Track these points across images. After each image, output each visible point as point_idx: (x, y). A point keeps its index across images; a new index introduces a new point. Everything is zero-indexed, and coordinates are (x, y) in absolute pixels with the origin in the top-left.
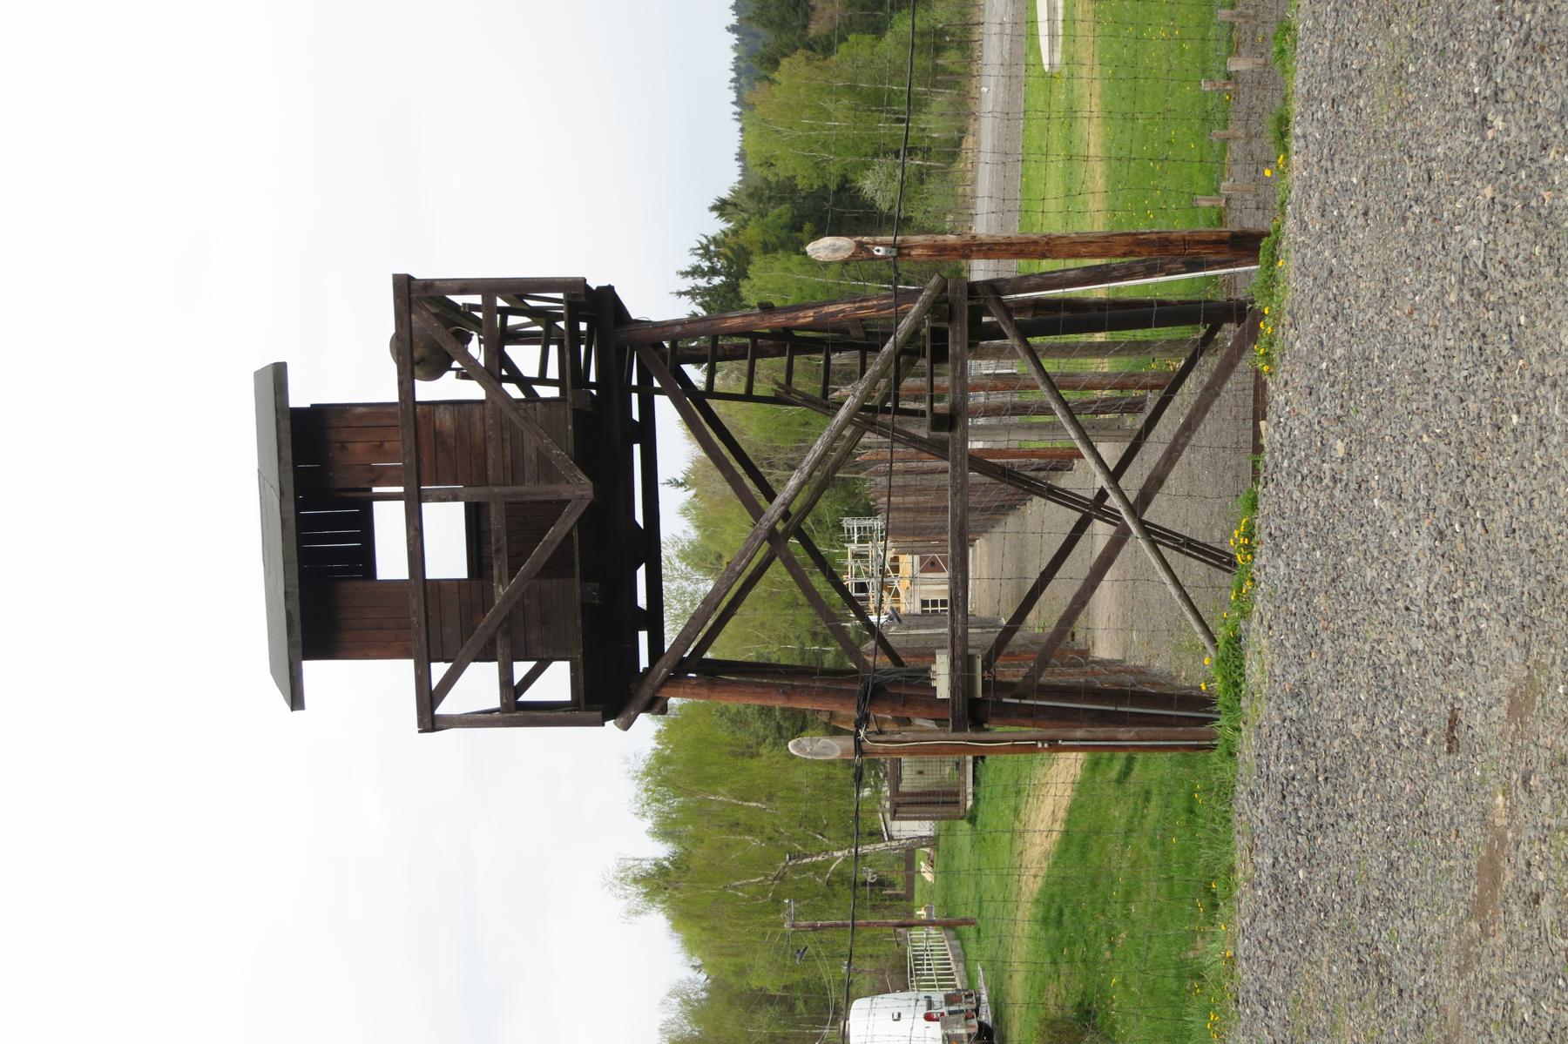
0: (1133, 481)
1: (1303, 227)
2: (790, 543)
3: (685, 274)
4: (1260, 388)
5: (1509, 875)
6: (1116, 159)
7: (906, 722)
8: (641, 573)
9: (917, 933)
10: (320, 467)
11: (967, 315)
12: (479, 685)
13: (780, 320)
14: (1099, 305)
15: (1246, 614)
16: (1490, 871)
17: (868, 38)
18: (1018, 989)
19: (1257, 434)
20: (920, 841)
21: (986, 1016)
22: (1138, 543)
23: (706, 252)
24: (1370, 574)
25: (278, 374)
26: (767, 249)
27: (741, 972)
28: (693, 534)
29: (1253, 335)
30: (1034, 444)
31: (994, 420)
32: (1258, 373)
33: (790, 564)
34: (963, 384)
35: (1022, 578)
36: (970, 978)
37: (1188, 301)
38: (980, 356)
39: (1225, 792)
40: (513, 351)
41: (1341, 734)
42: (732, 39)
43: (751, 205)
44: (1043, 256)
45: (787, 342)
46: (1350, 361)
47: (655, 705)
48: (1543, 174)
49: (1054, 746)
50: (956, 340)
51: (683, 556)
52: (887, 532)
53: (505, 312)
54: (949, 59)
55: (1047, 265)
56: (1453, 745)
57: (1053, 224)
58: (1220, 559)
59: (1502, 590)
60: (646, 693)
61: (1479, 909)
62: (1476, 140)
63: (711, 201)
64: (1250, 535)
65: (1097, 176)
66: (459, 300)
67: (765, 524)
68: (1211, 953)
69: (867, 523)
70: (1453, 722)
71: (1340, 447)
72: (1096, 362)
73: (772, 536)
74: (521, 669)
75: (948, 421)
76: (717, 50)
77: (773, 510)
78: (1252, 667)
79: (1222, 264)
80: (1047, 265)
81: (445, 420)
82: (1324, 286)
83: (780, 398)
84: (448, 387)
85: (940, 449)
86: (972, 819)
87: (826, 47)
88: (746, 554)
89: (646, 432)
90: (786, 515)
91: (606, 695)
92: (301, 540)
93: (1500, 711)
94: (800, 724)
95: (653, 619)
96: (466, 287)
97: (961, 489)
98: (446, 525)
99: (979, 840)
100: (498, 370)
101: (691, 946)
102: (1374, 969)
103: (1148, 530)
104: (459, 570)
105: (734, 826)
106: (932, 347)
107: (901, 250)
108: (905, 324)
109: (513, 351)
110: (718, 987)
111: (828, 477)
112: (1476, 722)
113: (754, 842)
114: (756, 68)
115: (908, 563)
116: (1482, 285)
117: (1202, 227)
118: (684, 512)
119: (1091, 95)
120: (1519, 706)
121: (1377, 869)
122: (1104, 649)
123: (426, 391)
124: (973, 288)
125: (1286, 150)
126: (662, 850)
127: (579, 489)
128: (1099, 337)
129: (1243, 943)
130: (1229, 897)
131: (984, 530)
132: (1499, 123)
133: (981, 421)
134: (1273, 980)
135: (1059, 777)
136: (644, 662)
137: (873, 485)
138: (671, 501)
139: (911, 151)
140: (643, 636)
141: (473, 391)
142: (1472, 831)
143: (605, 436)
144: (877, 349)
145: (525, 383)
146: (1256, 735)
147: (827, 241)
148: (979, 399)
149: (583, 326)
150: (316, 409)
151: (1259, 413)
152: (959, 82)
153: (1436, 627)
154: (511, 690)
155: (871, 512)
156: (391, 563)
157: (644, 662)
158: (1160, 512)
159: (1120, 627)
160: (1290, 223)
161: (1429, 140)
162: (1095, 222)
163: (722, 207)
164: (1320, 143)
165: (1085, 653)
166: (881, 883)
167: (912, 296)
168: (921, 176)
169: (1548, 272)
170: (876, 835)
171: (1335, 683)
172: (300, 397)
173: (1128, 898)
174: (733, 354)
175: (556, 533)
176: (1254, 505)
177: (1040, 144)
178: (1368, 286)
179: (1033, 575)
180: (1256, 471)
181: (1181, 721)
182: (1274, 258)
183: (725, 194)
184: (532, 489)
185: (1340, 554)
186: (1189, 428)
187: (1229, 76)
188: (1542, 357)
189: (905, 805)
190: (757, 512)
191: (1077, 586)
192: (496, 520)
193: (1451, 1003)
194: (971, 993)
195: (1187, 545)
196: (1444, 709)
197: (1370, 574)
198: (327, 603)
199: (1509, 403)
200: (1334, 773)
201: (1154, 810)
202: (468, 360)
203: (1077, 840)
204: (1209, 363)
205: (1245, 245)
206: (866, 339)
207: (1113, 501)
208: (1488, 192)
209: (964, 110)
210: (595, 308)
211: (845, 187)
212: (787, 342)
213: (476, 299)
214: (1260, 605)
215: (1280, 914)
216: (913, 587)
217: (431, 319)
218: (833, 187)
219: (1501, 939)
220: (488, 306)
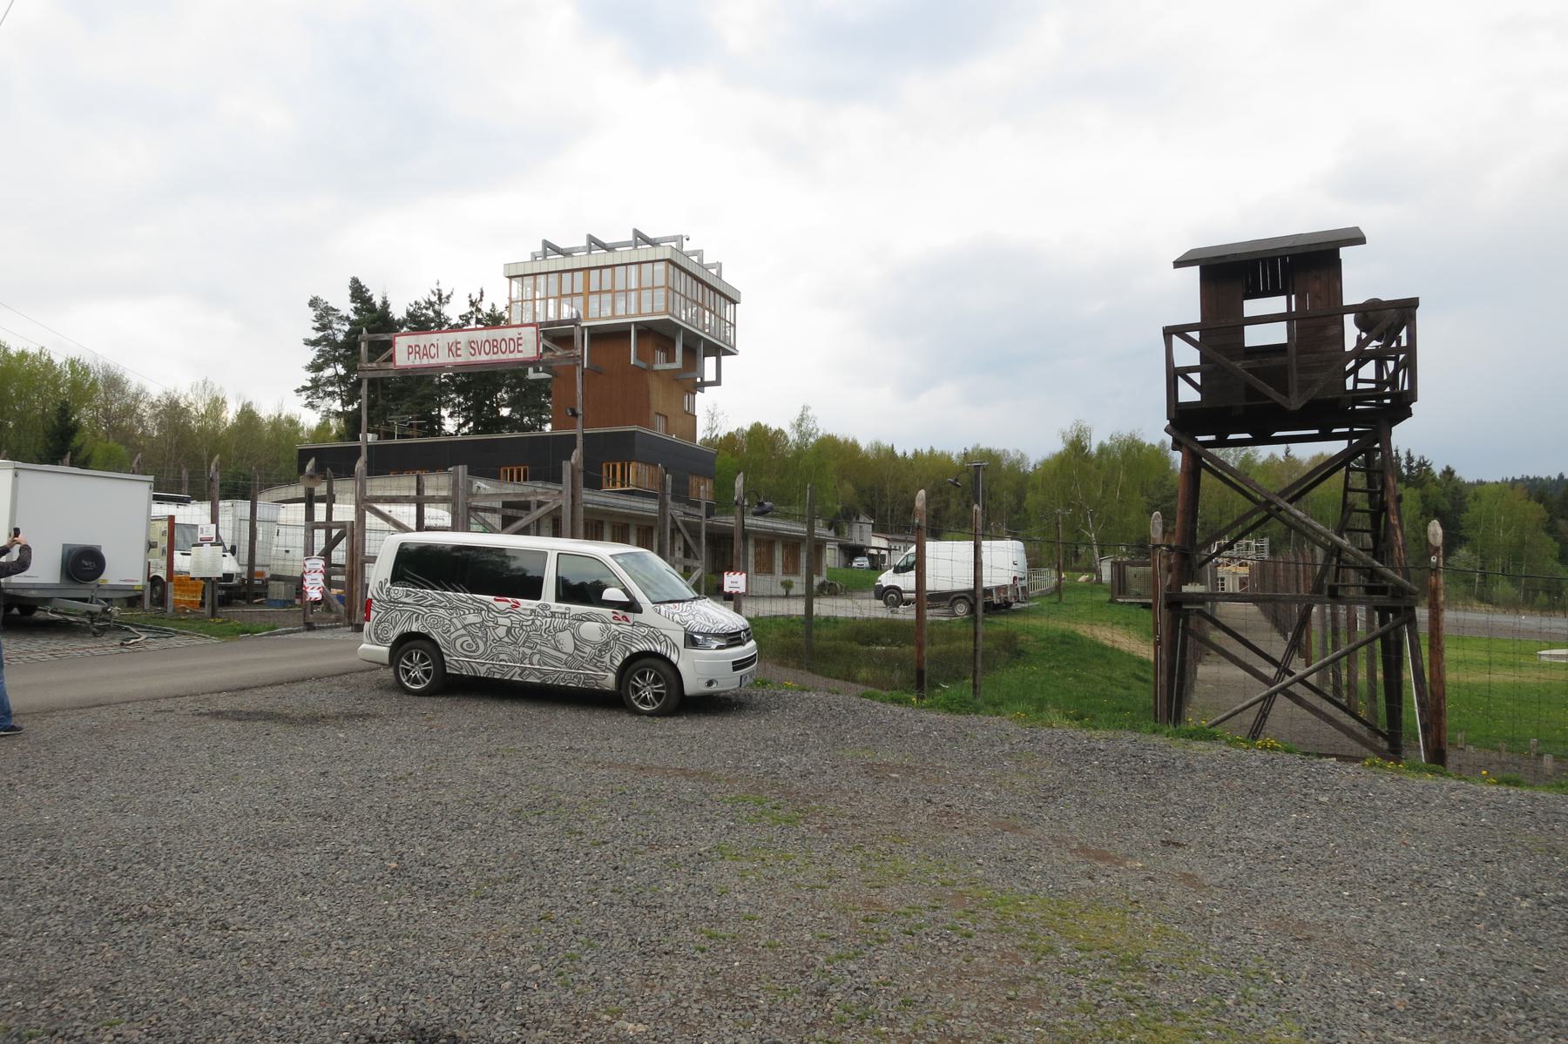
0: (1298, 689)
1: (1453, 790)
2: (1268, 510)
3: (1408, 453)
4: (1356, 760)
5: (1101, 866)
6: (1489, 689)
7: (1169, 570)
8: (1247, 436)
9: (1054, 573)
10: (1307, 266)
11: (1394, 606)
12: (1186, 355)
13: (1392, 506)
14: (1399, 676)
15: (1229, 743)
16: (1103, 857)
17: (1556, 554)
18: (1035, 622)
19: (1328, 756)
20: (1099, 574)
21: (1015, 606)
22: (1265, 691)
23: (1422, 464)
24: (1255, 809)
25: (1361, 240)
26: (1424, 498)
27: (1034, 488)
28: (1260, 461)
29: (1384, 757)
30: (1313, 638)
31: (1329, 617)
32: (1364, 759)
33: (1253, 512)
34: (1350, 603)
35: (1246, 629)
36: (1032, 599)
37: (1400, 723)
38: (1368, 611)
39: (1135, 728)
40: (1372, 364)
41: (1169, 787)
42: (1555, 476)
43: (1450, 489)
44: (1431, 647)
45: (1379, 510)
46: (1374, 808)
47: (1177, 445)
48: (1495, 926)
49: (1157, 644)
50: (1378, 599)
51: (1248, 456)
52: (1263, 561)
53: (1396, 359)
54: (1543, 598)
55: (1425, 650)
56: (1166, 843)
57: (1450, 653)
58: (1255, 733)
59: (1250, 877)
60: (1184, 440)
61: (1083, 849)
62: (1513, 890)
63: (1453, 467)
64: (1272, 748)
65: (1477, 678)
66: (1403, 334)
67: (1276, 499)
68: (1053, 716)
69: (1266, 550)
70: (1178, 845)
71: (1325, 799)
72: (1365, 672)
73: (1269, 502)
74: (1196, 377)
75: (1334, 595)
76: (1547, 469)
77: (1283, 503)
78: (1201, 745)
79: (1425, 743)
80: (1425, 650)
81: (1333, 331)
82: (1418, 798)
83: (1347, 507)
84: (1351, 334)
85: (1318, 589)
86: (1111, 601)
87: (1551, 530)
88: (1259, 489)
89: (1326, 436)
90: (1279, 509)
91: (1183, 420)
92: (1264, 260)
93: (1185, 870)
94: (1168, 517)
95: (1222, 443)
96: (1412, 337)
97: (1294, 600)
98: (1276, 334)
99: (1100, 604)
100: (1361, 356)
101: (1046, 463)
102: (1051, 795)
103: (1269, 699)
104: (1248, 343)
105: (1106, 484)
106: (1375, 587)
107: (1435, 570)
108: (1390, 572)
109: (1372, 364)
110: (1026, 476)
111: (1299, 532)
112: (1178, 856)
113: (1099, 494)
114: (1536, 490)
115: (1244, 571)
116: (1424, 884)
117: (1448, 735)
118: (1272, 456)
119: (1529, 677)
120: (1189, 879)
121: (1101, 800)
122: (1202, 671)
123: (1349, 319)
124: (1412, 609)
125: (1499, 783)
126: (1094, 448)
127: (1295, 403)
128: (1380, 675)
129: (1060, 732)
130: (1082, 726)
131: (1263, 610)
132: (1524, 904)
133: (1328, 611)
134: (1042, 745)
135: (1146, 652)
136: (1200, 438)
137: (1288, 553)
138: (1279, 450)
139: (1484, 576)
140: (1212, 438)
141: (1350, 344)
142: (1122, 849)
143: (1322, 416)
144: (1375, 557)
145: (1355, 370)
146: (1160, 744)
147: (1440, 531)
148: (1342, 610)
149: (1387, 401)
150: (1338, 263)
151: (1341, 758)
152: (1527, 602)
153: (1227, 841)
154: (1184, 372)
155: (1272, 552)
156: (1252, 307)
157: (1200, 438)
158: (1282, 702)
159: (1212, 674)
160: (1454, 783)
161: (1511, 864)
162: (1451, 676)
163: (1449, 473)
164: (1505, 803)
165: (1200, 661)
166: (1077, 556)
167: (1407, 576)
168: (1469, 581)
169: (1434, 921)
170: (1102, 554)
171: (1196, 787)
172: (1345, 253)
173: (1075, 676)
174: (1370, 483)
175: (1271, 391)
176: (1288, 751)
177: (1488, 646)
178: (1419, 822)
179: (1243, 634)
180: (1307, 754)
181: (1170, 707)
182: (1433, 772)
183: (1457, 474)
184: (1294, 378)
185: (1264, 794)
186: (1330, 720)
187: (1540, 755)
188: (1383, 912)
189: (1118, 569)
190: (1282, 494)
191: (1243, 658)
192: (1277, 360)
193: (1036, 831)
194: (1027, 599)
195: (1264, 715)
196: (1184, 841)
197: (1255, 809)
198: (1229, 275)
199: (1355, 891)
200: (1147, 782)
201: (1120, 691)
202: (1368, 341)
203: (1104, 654)
204: (1364, 731)
205: (1437, 756)
206: (1381, 549)
207: (1288, 679)
208: (1481, 894)
209: (1513, 606)
210: (1401, 406)
211: (1463, 540)
212: (1379, 510)
213: (1404, 343)
214: (1235, 752)
215: (1075, 751)
216: (1232, 573)
217: (1392, 320)
218: (1462, 533)
219: (1069, 858)
220: (1399, 350)
